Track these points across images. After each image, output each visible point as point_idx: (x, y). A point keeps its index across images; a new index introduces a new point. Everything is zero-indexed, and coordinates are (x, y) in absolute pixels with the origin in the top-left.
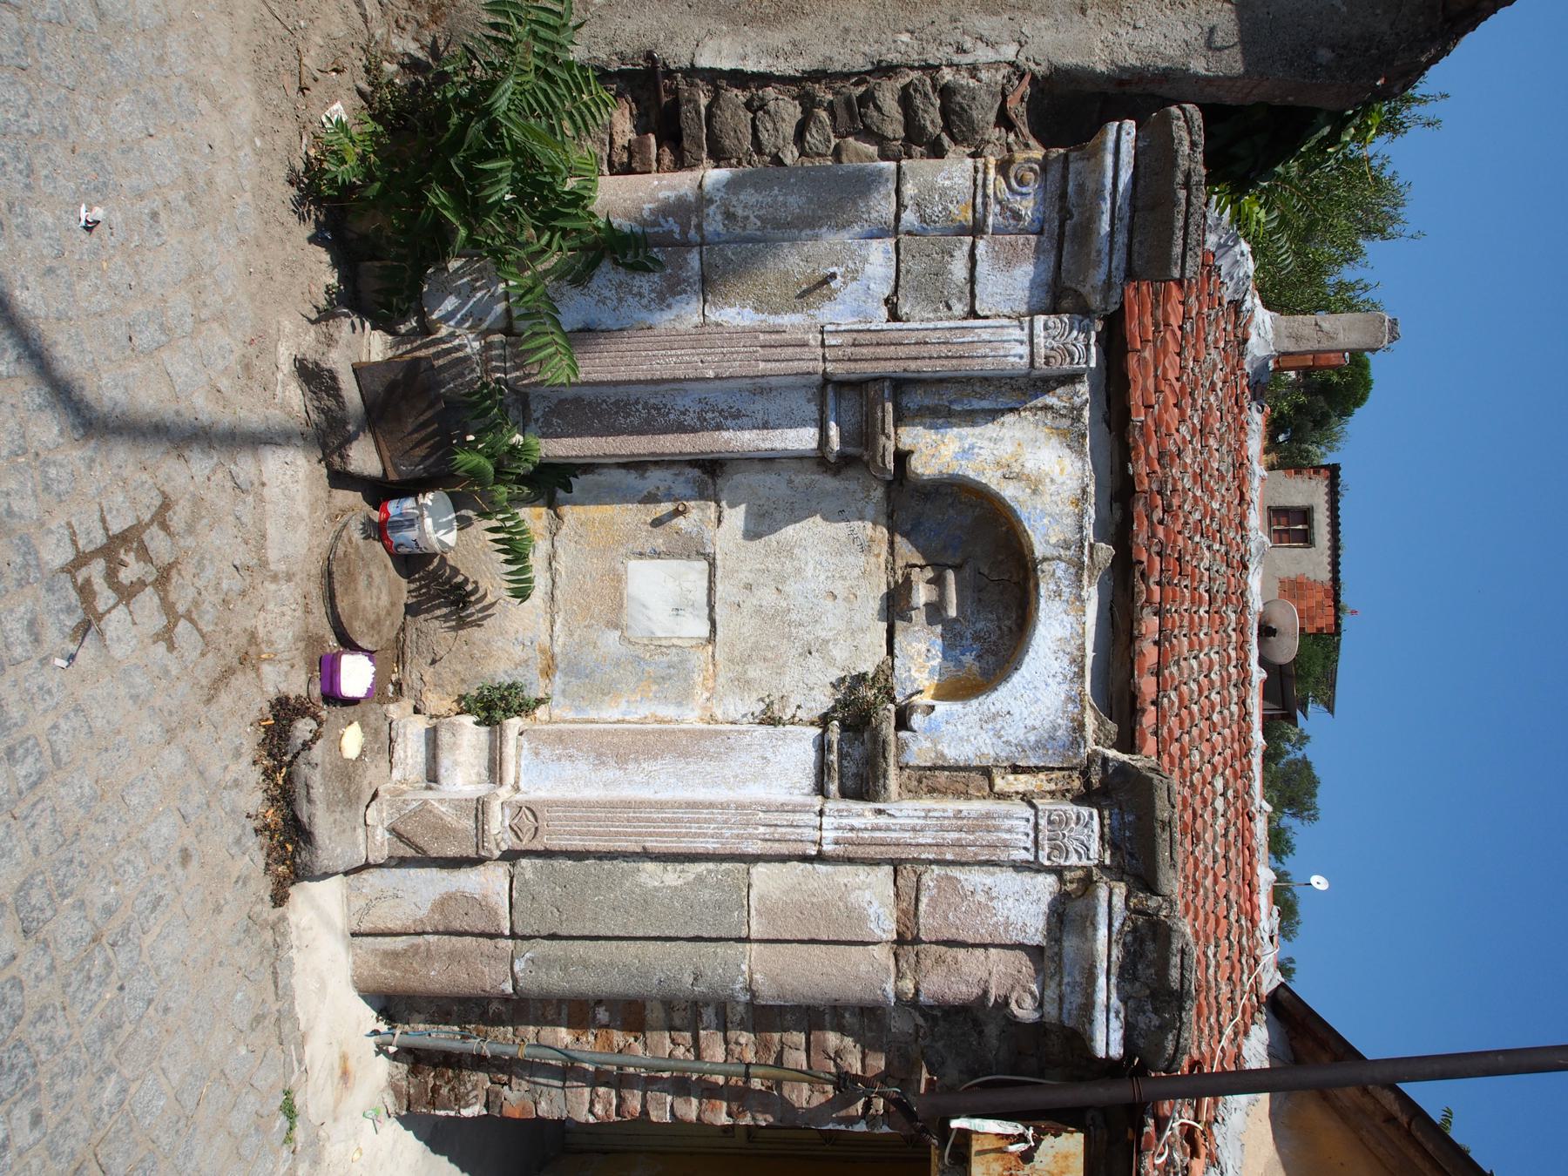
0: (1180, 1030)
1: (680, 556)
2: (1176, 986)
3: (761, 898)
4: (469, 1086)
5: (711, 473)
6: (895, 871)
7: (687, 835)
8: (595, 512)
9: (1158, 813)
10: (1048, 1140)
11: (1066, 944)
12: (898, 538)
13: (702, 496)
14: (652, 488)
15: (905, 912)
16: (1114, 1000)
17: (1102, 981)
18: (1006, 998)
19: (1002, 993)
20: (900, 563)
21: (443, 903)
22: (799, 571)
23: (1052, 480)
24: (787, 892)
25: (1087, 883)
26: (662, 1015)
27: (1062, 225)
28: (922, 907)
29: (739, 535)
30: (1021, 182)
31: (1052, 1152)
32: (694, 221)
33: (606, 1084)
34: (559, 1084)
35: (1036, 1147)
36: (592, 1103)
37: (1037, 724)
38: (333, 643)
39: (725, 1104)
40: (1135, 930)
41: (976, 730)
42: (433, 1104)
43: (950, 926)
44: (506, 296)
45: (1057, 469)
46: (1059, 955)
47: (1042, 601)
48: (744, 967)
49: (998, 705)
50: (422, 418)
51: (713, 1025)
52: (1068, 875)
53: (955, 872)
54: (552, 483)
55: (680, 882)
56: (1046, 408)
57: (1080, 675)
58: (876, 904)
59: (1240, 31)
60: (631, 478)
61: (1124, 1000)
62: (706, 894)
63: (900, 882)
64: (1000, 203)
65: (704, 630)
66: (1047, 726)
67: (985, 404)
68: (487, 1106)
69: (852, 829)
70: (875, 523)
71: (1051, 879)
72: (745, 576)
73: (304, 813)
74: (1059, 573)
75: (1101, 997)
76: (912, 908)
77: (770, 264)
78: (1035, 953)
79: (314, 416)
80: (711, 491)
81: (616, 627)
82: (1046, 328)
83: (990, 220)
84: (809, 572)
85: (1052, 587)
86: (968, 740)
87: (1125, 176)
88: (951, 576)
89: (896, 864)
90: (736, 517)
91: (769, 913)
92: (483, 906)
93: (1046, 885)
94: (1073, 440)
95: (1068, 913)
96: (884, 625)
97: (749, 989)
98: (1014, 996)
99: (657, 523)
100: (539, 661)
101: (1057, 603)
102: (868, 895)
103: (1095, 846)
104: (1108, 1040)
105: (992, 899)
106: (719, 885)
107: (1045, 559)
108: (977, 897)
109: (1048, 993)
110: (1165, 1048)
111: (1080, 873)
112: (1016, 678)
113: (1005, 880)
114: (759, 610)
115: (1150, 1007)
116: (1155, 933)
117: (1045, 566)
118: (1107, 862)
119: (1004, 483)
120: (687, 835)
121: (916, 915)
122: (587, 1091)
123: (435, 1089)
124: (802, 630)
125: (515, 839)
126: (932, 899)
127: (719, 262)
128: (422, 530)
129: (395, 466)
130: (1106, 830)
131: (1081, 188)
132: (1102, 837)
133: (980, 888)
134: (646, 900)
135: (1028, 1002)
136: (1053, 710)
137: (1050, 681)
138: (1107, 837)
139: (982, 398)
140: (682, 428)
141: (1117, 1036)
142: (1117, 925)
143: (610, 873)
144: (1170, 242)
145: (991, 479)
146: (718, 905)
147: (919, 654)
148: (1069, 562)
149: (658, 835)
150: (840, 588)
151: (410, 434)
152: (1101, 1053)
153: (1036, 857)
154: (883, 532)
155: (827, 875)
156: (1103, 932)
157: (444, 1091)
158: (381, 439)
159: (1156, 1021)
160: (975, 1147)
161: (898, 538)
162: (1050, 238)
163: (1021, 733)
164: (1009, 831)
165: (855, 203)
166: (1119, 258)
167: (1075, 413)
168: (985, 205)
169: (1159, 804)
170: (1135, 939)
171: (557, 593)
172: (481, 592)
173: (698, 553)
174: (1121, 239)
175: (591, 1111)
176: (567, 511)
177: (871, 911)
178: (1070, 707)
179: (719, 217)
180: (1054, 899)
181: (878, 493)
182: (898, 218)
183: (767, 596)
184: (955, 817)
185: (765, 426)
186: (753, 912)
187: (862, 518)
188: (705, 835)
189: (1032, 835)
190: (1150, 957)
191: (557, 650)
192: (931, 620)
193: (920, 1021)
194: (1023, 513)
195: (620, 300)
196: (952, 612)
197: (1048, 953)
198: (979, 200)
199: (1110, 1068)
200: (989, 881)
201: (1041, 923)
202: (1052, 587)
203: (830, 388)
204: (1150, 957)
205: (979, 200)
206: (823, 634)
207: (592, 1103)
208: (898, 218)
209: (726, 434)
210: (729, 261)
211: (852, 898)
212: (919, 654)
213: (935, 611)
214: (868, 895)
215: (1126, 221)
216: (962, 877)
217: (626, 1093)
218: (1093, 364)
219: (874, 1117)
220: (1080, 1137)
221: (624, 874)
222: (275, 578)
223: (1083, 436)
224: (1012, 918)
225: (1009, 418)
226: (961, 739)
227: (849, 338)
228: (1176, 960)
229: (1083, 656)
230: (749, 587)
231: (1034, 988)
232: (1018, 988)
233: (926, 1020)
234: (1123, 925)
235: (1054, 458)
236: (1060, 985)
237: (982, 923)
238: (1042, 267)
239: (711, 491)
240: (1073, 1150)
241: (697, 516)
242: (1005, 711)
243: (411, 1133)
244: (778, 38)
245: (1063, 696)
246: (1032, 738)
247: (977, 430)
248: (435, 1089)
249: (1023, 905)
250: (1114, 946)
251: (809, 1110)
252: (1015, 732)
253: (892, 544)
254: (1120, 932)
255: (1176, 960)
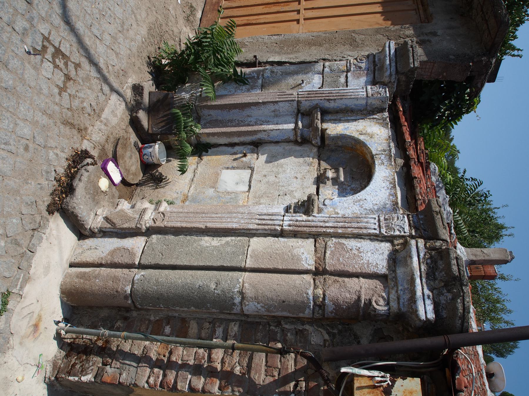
0: (463, 296)
1: (242, 168)
2: (457, 274)
3: (253, 251)
4: (91, 364)
5: (256, 145)
6: (315, 241)
7: (225, 222)
8: (214, 157)
9: (434, 209)
10: (399, 382)
11: (398, 272)
12: (322, 162)
13: (253, 152)
14: (235, 151)
15: (319, 258)
16: (427, 292)
17: (418, 281)
18: (370, 300)
19: (367, 298)
20: (322, 168)
21: (113, 252)
22: (285, 171)
23: (377, 135)
24: (265, 249)
25: (406, 244)
26: (196, 331)
27: (374, 68)
28: (328, 255)
29: (264, 162)
30: (361, 60)
31: (402, 389)
32: (261, 73)
33: (160, 368)
34: (135, 364)
35: (393, 386)
36: (149, 377)
37: (378, 203)
38: (111, 156)
39: (218, 382)
40: (431, 257)
41: (352, 205)
42: (69, 374)
43: (340, 264)
44: (201, 92)
45: (379, 132)
46: (396, 277)
47: (377, 166)
48: (241, 280)
49: (361, 197)
50: (165, 113)
51: (221, 336)
52: (396, 242)
53: (343, 241)
54: (201, 149)
55: (219, 244)
56: (374, 118)
57: (394, 187)
58: (305, 254)
59: (425, 53)
60: (229, 149)
61: (431, 290)
62: (229, 249)
63: (317, 245)
64: (355, 65)
65: (247, 189)
66: (382, 203)
67: (352, 118)
68: (95, 378)
69: (297, 221)
70: (313, 158)
71: (388, 245)
72: (264, 172)
73: (76, 183)
74: (382, 158)
75: (419, 293)
76: (322, 256)
77: (283, 81)
78: (382, 278)
79: (132, 102)
80: (256, 151)
81: (213, 188)
82: (371, 88)
83: (352, 69)
84: (288, 171)
85: (380, 162)
86: (348, 208)
87: (393, 51)
88: (341, 169)
89: (315, 236)
90: (263, 158)
91: (255, 257)
92: (131, 253)
93: (386, 247)
94: (385, 125)
95: (397, 259)
96: (316, 186)
97: (241, 293)
98: (374, 299)
99: (235, 160)
100: (182, 198)
101: (382, 166)
102: (302, 250)
103: (407, 228)
104: (426, 310)
105: (360, 252)
106: (235, 246)
107: (376, 154)
108: (353, 252)
109: (392, 296)
110: (457, 309)
111: (401, 241)
112: (368, 188)
113: (366, 245)
114: (268, 182)
115: (445, 291)
116: (441, 256)
117: (377, 156)
118: (414, 234)
119: (360, 136)
120: (225, 222)
121: (324, 259)
122: (148, 370)
123: (74, 365)
124: (283, 188)
125: (153, 223)
126: (332, 251)
127: (268, 81)
128: (154, 148)
129: (152, 128)
130: (411, 222)
131: (380, 59)
132: (410, 225)
133: (354, 248)
134: (202, 251)
135: (382, 302)
136: (384, 198)
137: (382, 189)
138: (412, 224)
139: (351, 116)
140: (249, 125)
141: (430, 308)
142: (422, 255)
143: (189, 240)
144: (409, 59)
145: (356, 135)
146: (234, 253)
147: (329, 194)
148: (386, 155)
149: (213, 222)
150: (299, 176)
151: (160, 118)
152: (423, 317)
153: (380, 232)
154: (316, 161)
155: (284, 242)
156: (415, 259)
157: (78, 366)
158: (150, 120)
159: (450, 296)
160: (357, 384)
161: (322, 162)
162: (371, 71)
163: (371, 206)
164: (367, 222)
165: (310, 67)
166: (393, 68)
167: (384, 119)
168: (350, 65)
169: (433, 206)
170: (432, 262)
171: (195, 179)
172: (168, 178)
173: (248, 167)
174: (393, 64)
175: (147, 382)
176: (205, 158)
177: (303, 257)
178: (391, 197)
179: (269, 72)
180: (390, 253)
181: (315, 150)
182: (323, 70)
183: (272, 178)
184: (342, 217)
185: (277, 124)
186: (248, 256)
187: (309, 157)
188: (233, 222)
189: (377, 224)
190: (441, 267)
191: (189, 194)
192: (333, 184)
193: (327, 337)
194: (368, 143)
195: (235, 91)
196: (342, 179)
197: (390, 277)
198: (348, 64)
199: (428, 328)
200: (359, 245)
201: (385, 263)
202: (380, 162)
203: (300, 115)
204: (441, 267)
205: (348, 64)
206: (292, 189)
207: (149, 377)
208: (323, 70)
209: (263, 126)
210: (271, 81)
211: (295, 251)
212: (329, 194)
213: (335, 181)
214: (302, 250)
215: (394, 60)
216: (346, 243)
217: (168, 372)
218: (388, 95)
219: (300, 392)
220: (418, 380)
221: (195, 241)
222: (101, 122)
223: (388, 124)
224: (370, 261)
225: (360, 121)
226: (346, 208)
227: (307, 93)
228: (454, 262)
229: (395, 182)
230: (265, 176)
231: (384, 294)
232: (375, 295)
233: (330, 336)
234: (425, 255)
235: (378, 129)
236: (397, 292)
237: (356, 263)
238: (369, 78)
239: (256, 151)
240: (415, 389)
241: (250, 158)
242: (364, 198)
243: (56, 342)
244: (292, 56)
245: (388, 194)
246: (376, 208)
247: (350, 123)
248: (74, 365)
249: (375, 256)
250: (422, 264)
251: (264, 386)
252: (368, 205)
253: (319, 164)
254: (424, 258)
255: (454, 262)
